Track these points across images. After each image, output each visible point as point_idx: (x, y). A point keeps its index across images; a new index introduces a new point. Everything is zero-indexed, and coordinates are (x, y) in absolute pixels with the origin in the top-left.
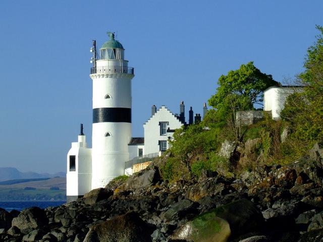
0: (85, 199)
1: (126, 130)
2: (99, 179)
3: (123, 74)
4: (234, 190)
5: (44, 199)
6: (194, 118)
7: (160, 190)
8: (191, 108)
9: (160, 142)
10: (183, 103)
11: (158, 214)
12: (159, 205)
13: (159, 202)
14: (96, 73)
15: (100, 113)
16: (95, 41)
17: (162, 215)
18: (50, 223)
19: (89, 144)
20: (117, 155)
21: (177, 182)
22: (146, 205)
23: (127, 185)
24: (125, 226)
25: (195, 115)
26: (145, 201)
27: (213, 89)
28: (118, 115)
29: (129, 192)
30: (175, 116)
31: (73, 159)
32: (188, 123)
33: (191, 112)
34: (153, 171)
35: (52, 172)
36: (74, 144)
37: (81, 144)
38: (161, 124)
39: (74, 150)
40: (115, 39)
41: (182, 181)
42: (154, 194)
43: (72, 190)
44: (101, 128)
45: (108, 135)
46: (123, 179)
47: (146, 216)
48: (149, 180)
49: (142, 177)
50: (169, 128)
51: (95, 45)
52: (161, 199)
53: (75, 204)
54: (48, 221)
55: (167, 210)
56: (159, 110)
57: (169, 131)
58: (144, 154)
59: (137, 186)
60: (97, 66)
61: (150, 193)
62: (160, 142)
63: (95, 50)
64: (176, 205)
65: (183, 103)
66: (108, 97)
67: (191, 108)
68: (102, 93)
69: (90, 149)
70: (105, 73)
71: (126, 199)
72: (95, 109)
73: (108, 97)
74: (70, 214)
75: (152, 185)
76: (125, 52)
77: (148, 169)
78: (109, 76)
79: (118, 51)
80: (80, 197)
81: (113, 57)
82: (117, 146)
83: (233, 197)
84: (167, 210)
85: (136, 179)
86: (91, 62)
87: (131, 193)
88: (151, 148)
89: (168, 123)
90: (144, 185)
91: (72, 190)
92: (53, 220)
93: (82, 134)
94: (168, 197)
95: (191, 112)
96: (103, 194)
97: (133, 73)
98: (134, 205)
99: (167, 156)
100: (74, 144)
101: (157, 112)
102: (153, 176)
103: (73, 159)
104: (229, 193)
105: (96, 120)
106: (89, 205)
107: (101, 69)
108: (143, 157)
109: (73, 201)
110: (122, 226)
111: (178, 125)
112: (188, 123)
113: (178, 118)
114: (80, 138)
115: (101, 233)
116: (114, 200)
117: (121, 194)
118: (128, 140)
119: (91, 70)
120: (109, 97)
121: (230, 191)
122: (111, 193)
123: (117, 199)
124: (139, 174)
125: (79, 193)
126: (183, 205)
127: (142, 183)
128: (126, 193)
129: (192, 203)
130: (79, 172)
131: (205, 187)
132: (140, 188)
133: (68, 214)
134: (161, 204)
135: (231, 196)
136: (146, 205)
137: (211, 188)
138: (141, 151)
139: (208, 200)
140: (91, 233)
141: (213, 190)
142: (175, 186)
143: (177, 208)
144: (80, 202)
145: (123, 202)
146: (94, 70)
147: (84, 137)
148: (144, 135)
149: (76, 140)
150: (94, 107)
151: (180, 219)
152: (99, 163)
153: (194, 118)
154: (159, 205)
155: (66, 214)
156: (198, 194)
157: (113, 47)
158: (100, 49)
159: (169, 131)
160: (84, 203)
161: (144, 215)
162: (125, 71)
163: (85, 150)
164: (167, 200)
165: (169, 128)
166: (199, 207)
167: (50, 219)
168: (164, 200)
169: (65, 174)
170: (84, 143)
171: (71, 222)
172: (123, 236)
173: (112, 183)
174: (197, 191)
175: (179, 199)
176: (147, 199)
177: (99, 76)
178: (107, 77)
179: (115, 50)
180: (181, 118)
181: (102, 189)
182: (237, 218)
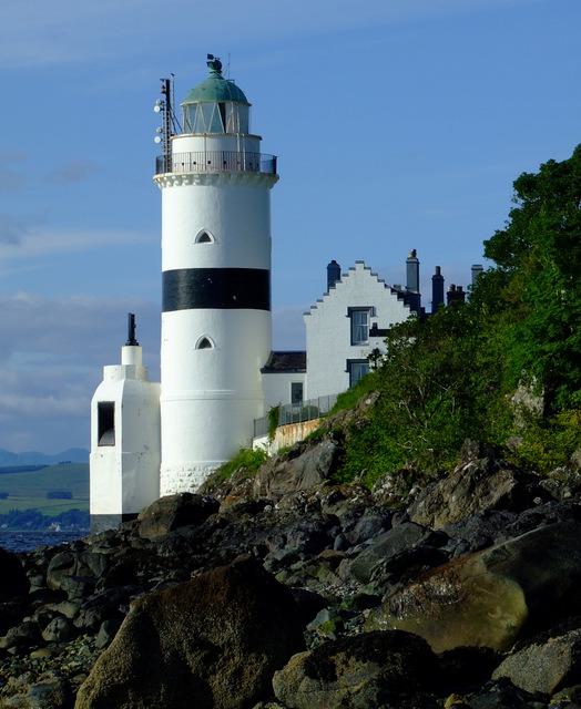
0: (140, 522)
1: (253, 332)
2: (181, 468)
3: (246, 174)
4: (546, 496)
5: (29, 524)
6: (445, 296)
7: (344, 498)
8: (438, 269)
9: (350, 363)
10: (414, 253)
11: (334, 563)
12: (338, 540)
13: (339, 532)
14: (170, 171)
15: (183, 285)
16: (168, 82)
17: (345, 567)
18: (33, 589)
19: (152, 372)
20: (225, 405)
21: (394, 475)
22: (302, 539)
23: (259, 484)
24: (229, 599)
25: (447, 289)
26: (299, 529)
27: (497, 210)
28: (231, 288)
29: (263, 503)
30: (393, 291)
31: (106, 412)
32: (428, 310)
33: (438, 281)
34: (328, 446)
35: (49, 449)
36: (109, 370)
37: (129, 371)
38: (352, 312)
39: (110, 388)
40: (226, 74)
41: (406, 472)
42: (327, 510)
43: (106, 496)
44: (181, 328)
45: (204, 344)
46: (246, 463)
47: (300, 569)
48: (319, 470)
49: (298, 462)
50: (375, 325)
51: (167, 93)
52: (345, 525)
53: (112, 539)
54: (29, 585)
55: (357, 554)
56: (347, 275)
57: (376, 332)
58: (306, 397)
59: (284, 486)
60: (174, 152)
61: (316, 507)
62: (350, 363)
63: (167, 106)
64: (383, 538)
65: (414, 253)
66: (204, 238)
67: (438, 269)
68: (183, 231)
69: (153, 384)
70: (196, 171)
71: (248, 523)
72: (165, 272)
73: (204, 238)
74: (90, 566)
75: (326, 485)
76: (254, 113)
77: (315, 439)
78: (208, 181)
79: (231, 110)
80: (126, 517)
81: (218, 128)
82: (226, 373)
83: (538, 518)
84: (357, 554)
85: (281, 466)
86: (157, 140)
87: (267, 508)
88: (325, 380)
89: (370, 310)
90: (305, 484)
91: (106, 496)
92: (44, 583)
93: (132, 342)
94: (364, 519)
95: (438, 281)
96: (187, 508)
97: (275, 172)
98: (270, 539)
99: (369, 402)
100: (109, 370)
101: (342, 278)
102: (328, 458)
103: (106, 412)
104: (534, 505)
105: (171, 304)
106: (147, 541)
107: (187, 160)
108: (305, 405)
109: (107, 528)
110: (221, 598)
111: (398, 313)
112: (428, 310)
113: (401, 296)
114: (126, 351)
115: (161, 617)
116: (216, 526)
117: (240, 510)
118: (261, 361)
119: (158, 162)
120: (209, 240)
121: (537, 500)
122: (213, 506)
123: (224, 523)
124: (292, 452)
125: (94, 516)
126: (404, 538)
127: (299, 479)
128: (254, 508)
129: (427, 534)
130: (123, 449)
131: (461, 490)
132: (293, 492)
133: (85, 565)
134: (343, 538)
135: (536, 515)
136: (302, 539)
137: (479, 490)
138: (297, 391)
139: (473, 523)
140: (134, 619)
141: (486, 493)
142: (388, 485)
143: (386, 547)
144: (127, 533)
145: (241, 532)
146: (164, 164)
147: (139, 349)
148: (303, 336)
149: (118, 361)
150: (167, 265)
151: (393, 580)
152: (173, 422)
153: (445, 296)
154: (338, 540)
155: (79, 565)
156: (445, 511)
157: (218, 97)
158: (180, 103)
159: (376, 332)
160: (136, 535)
161: (294, 567)
162: (253, 165)
163: (141, 385)
164: (360, 525)
165: (375, 325)
166: (445, 544)
167: (35, 580)
168: (352, 527)
169: (85, 454)
170: (139, 368)
171: (88, 590)
172: (223, 625)
173: (216, 481)
174: (438, 505)
175: (395, 524)
176: (304, 524)
177: (180, 178)
178: (191, 183)
179: (222, 107)
180: (410, 298)
181: (187, 496)
182: (546, 576)
